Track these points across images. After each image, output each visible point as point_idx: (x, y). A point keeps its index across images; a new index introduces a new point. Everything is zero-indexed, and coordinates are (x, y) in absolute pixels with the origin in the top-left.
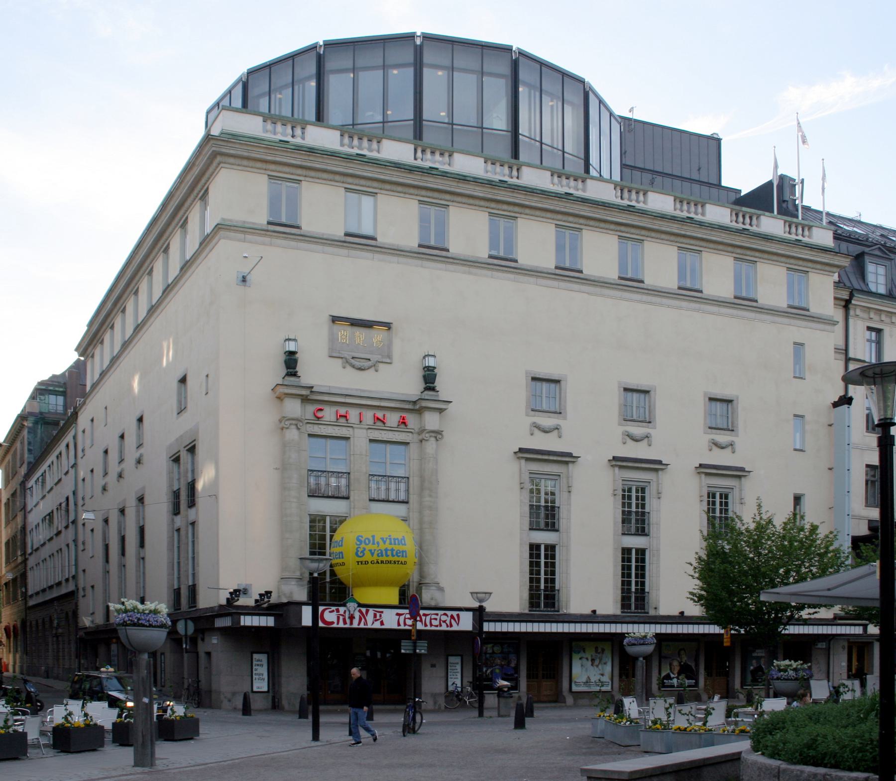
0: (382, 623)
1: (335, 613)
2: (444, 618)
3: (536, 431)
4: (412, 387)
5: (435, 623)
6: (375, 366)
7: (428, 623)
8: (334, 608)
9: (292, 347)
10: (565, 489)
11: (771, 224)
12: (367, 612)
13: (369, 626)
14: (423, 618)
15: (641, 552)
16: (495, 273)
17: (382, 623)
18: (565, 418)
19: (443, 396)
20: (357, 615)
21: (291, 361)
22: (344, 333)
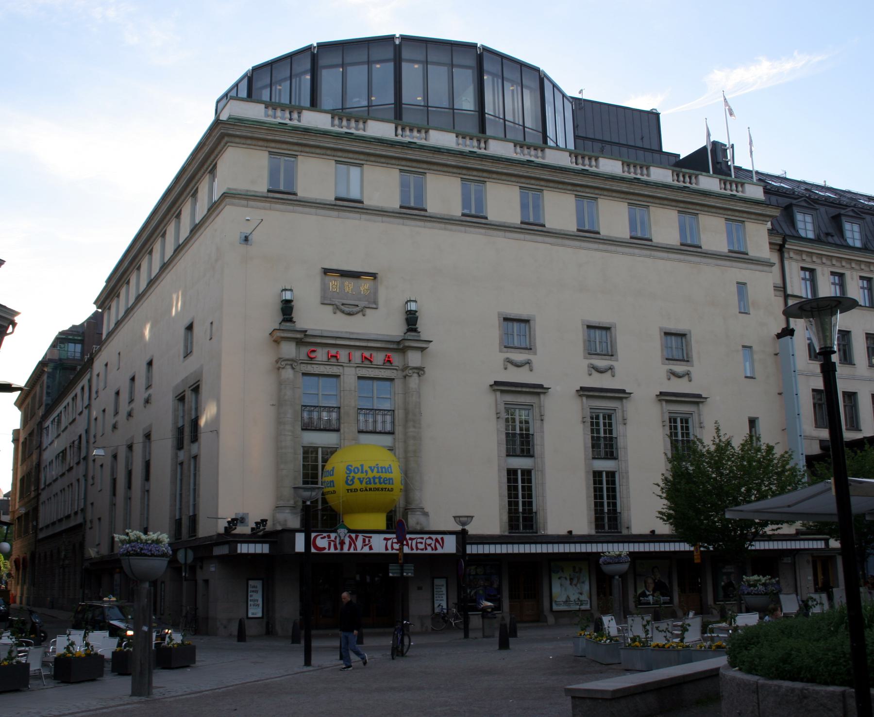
0: (371, 548)
1: (326, 539)
2: (429, 541)
3: (509, 366)
4: (395, 329)
5: (421, 546)
6: (362, 311)
7: (414, 547)
8: (325, 534)
9: (288, 296)
10: (538, 417)
11: (709, 183)
12: (357, 537)
13: (359, 551)
14: (410, 542)
15: (611, 475)
16: (342, 214)
17: (371, 548)
18: (535, 353)
19: (424, 337)
20: (347, 540)
21: (287, 309)
22: (334, 283)
